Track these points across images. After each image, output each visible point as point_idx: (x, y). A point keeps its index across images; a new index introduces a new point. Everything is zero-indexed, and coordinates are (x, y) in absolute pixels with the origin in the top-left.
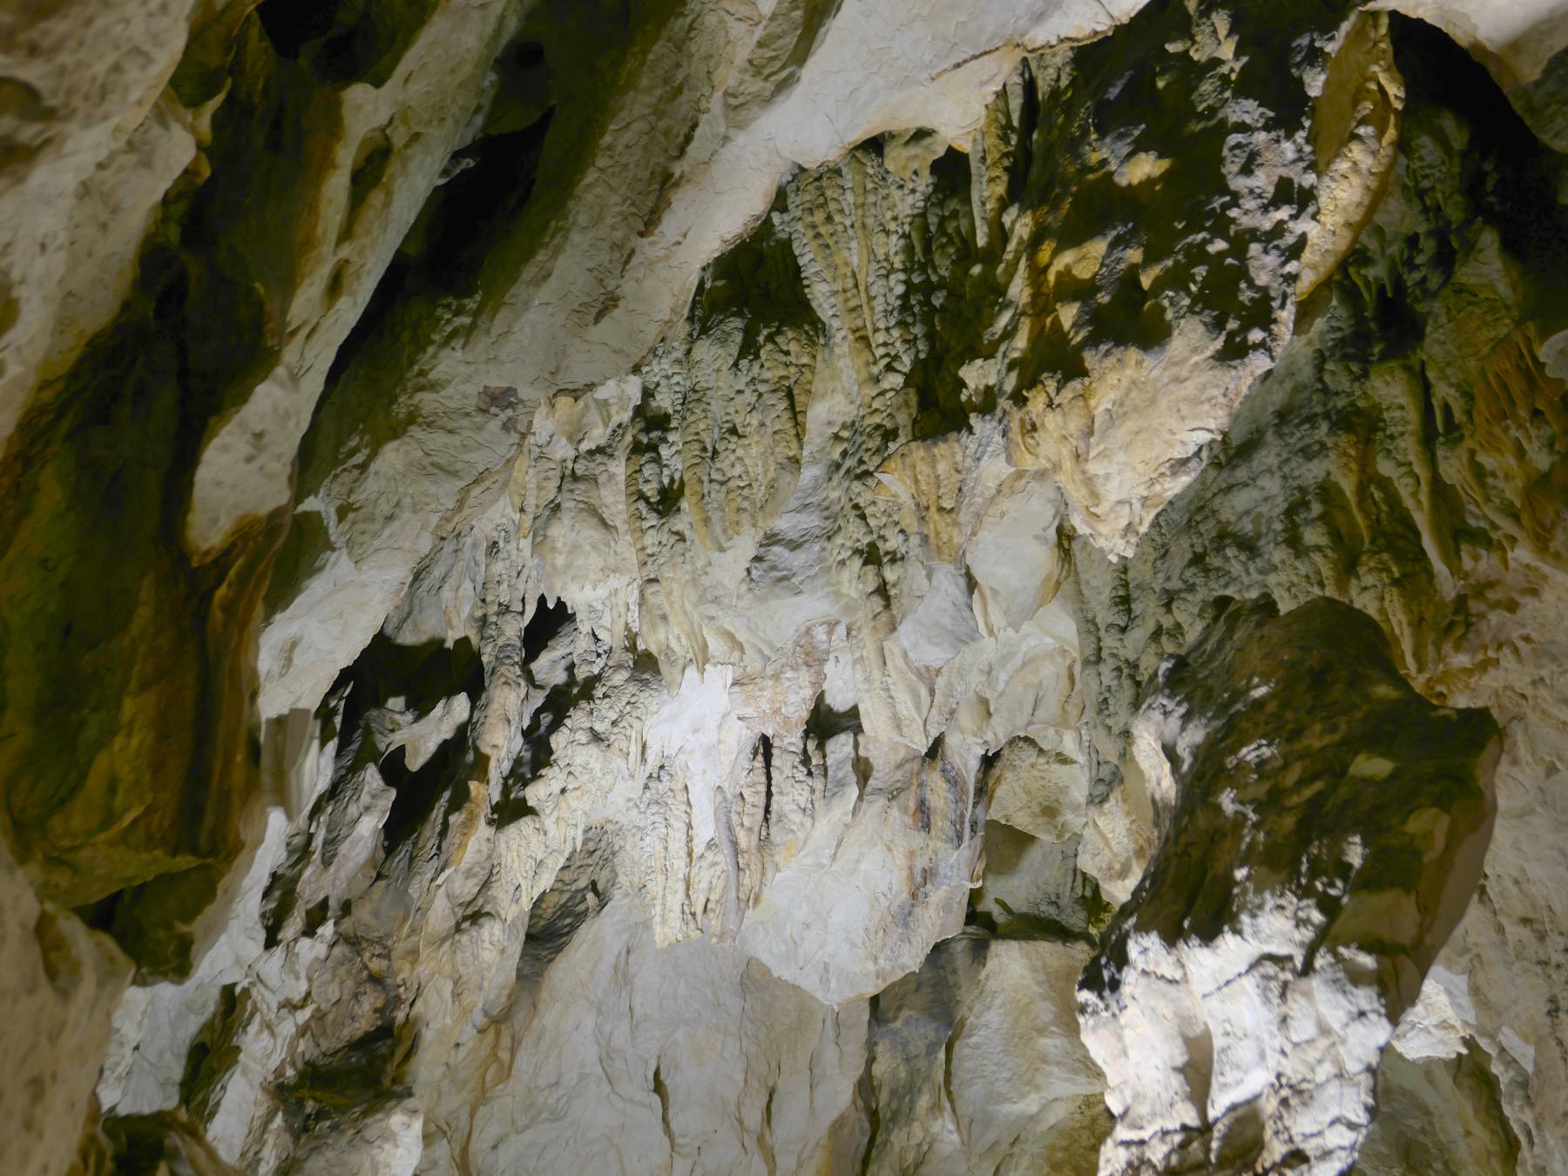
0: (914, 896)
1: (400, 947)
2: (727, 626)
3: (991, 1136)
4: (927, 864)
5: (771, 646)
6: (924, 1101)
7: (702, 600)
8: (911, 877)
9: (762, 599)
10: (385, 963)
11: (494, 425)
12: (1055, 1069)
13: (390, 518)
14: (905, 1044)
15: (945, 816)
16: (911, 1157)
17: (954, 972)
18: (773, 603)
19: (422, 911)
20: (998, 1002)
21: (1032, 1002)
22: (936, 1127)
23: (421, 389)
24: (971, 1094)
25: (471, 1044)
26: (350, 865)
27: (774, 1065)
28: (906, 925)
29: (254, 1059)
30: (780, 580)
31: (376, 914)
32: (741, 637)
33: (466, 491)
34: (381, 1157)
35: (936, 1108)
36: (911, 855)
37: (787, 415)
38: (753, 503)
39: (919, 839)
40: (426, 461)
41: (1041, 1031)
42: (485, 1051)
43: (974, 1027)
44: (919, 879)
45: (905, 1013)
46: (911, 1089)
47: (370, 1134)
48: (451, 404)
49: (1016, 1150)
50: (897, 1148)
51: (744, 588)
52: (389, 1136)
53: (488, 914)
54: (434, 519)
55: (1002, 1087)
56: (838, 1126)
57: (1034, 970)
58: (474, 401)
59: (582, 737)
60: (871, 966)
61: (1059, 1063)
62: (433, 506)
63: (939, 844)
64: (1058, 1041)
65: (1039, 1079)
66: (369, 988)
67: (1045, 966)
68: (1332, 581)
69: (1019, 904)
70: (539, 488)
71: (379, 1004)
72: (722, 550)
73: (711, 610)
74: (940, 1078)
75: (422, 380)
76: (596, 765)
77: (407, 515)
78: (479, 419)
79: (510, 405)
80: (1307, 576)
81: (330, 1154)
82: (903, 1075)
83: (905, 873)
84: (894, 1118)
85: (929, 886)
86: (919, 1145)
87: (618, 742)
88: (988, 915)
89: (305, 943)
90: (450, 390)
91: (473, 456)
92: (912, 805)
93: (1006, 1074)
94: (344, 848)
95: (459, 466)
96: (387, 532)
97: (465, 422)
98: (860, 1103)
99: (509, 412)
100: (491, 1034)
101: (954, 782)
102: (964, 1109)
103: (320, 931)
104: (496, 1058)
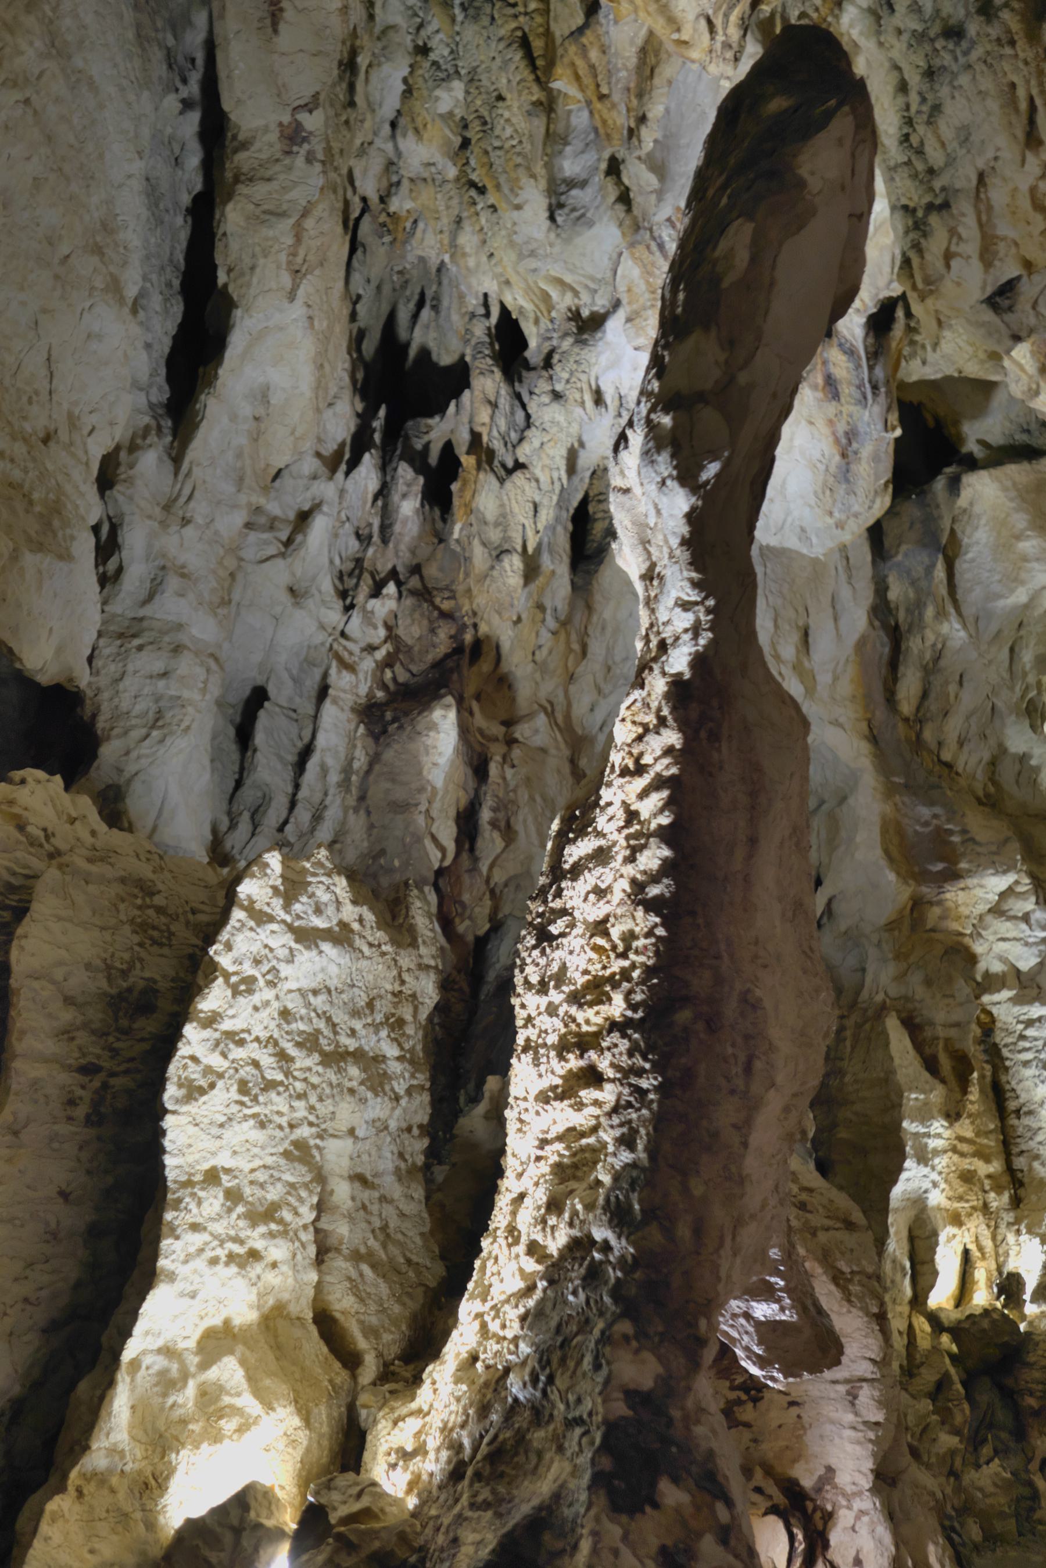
0: (844, 455)
1: (460, 588)
2: (553, 273)
3: (994, 628)
4: (847, 428)
5: (593, 279)
6: (930, 612)
7: (521, 257)
8: (837, 441)
9: (568, 241)
10: (452, 602)
11: (300, 161)
12: (1035, 565)
13: (253, 268)
14: (908, 572)
15: (850, 383)
16: (928, 656)
17: (938, 506)
18: (578, 241)
19: (468, 559)
20: (983, 522)
21: (1008, 515)
22: (945, 628)
23: (235, 151)
24: (972, 597)
25: (549, 644)
26: (407, 539)
27: (801, 610)
28: (847, 481)
29: (345, 691)
30: (578, 218)
31: (441, 569)
32: (568, 279)
33: (298, 225)
34: (429, 742)
35: (941, 614)
36: (831, 422)
37: (523, 64)
38: (525, 157)
39: (831, 408)
40: (258, 211)
41: (1018, 537)
42: (562, 646)
43: (969, 545)
44: (844, 441)
45: (904, 548)
46: (917, 607)
47: (419, 728)
48: (264, 156)
49: (1022, 632)
50: (916, 651)
51: (552, 235)
52: (433, 727)
53: (507, 551)
54: (283, 257)
55: (996, 588)
56: (861, 645)
57: (1005, 489)
58: (278, 146)
59: (546, 399)
60: (830, 521)
61: (1038, 560)
62: (276, 247)
63: (852, 408)
64: (1034, 542)
65: (1023, 575)
66: (441, 622)
67: (1014, 484)
68: (1022, 34)
69: (996, 439)
70: (448, 207)
71: (453, 632)
72: (518, 207)
73: (532, 263)
74: (943, 590)
75: (235, 144)
76: (560, 418)
77: (262, 261)
78: (287, 161)
79: (305, 140)
80: (998, 40)
81: (396, 746)
82: (911, 595)
83: (831, 439)
84: (909, 631)
85: (855, 445)
86: (934, 645)
87: (573, 395)
88: (970, 455)
89: (373, 603)
90: (257, 145)
91: (293, 195)
92: (820, 380)
93: (997, 577)
94: (397, 528)
95: (285, 207)
96: (255, 280)
97: (277, 168)
98: (877, 623)
99: (306, 146)
100: (562, 636)
101: (851, 352)
102: (968, 611)
103: (385, 591)
104: (571, 650)
